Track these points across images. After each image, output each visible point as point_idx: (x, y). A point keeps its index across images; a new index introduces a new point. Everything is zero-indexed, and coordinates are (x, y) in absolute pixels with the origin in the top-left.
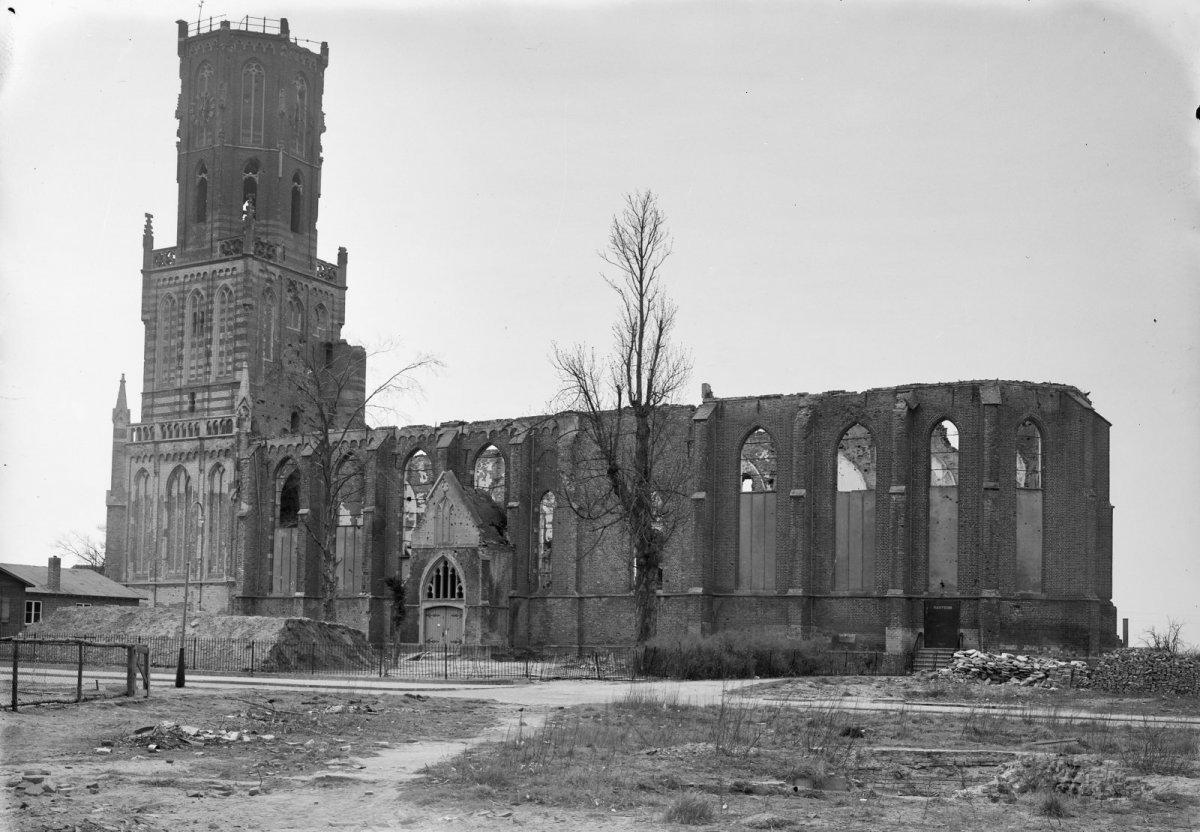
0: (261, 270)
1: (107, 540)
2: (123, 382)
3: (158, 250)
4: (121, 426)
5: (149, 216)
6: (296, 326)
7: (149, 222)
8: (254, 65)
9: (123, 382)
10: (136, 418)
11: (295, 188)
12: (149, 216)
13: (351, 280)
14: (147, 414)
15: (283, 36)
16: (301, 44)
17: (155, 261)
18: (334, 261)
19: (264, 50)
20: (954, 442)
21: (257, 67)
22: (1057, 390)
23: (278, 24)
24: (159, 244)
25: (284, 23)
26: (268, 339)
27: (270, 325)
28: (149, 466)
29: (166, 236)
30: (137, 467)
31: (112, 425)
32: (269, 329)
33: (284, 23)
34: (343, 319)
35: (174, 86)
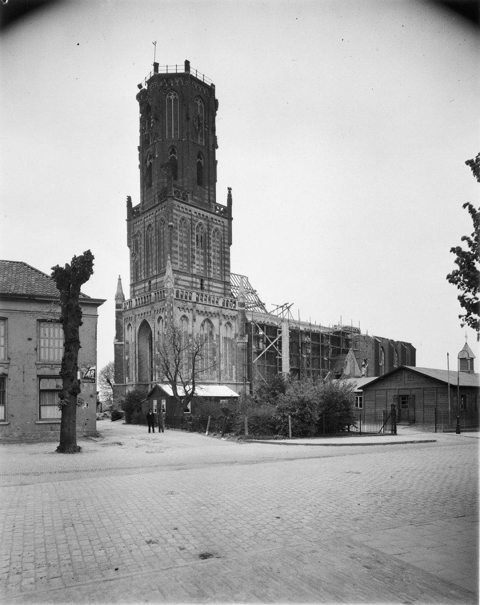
1: (115, 361)
2: (120, 279)
3: (228, 205)
4: (119, 302)
5: (230, 189)
7: (230, 192)
9: (120, 279)
10: (127, 297)
11: (199, 162)
12: (230, 189)
13: (234, 214)
14: (133, 293)
15: (187, 72)
17: (133, 213)
18: (226, 205)
19: (200, 90)
21: (175, 95)
24: (134, 205)
25: (187, 63)
28: (189, 315)
29: (136, 201)
30: (182, 313)
33: (187, 63)
34: (21, 263)
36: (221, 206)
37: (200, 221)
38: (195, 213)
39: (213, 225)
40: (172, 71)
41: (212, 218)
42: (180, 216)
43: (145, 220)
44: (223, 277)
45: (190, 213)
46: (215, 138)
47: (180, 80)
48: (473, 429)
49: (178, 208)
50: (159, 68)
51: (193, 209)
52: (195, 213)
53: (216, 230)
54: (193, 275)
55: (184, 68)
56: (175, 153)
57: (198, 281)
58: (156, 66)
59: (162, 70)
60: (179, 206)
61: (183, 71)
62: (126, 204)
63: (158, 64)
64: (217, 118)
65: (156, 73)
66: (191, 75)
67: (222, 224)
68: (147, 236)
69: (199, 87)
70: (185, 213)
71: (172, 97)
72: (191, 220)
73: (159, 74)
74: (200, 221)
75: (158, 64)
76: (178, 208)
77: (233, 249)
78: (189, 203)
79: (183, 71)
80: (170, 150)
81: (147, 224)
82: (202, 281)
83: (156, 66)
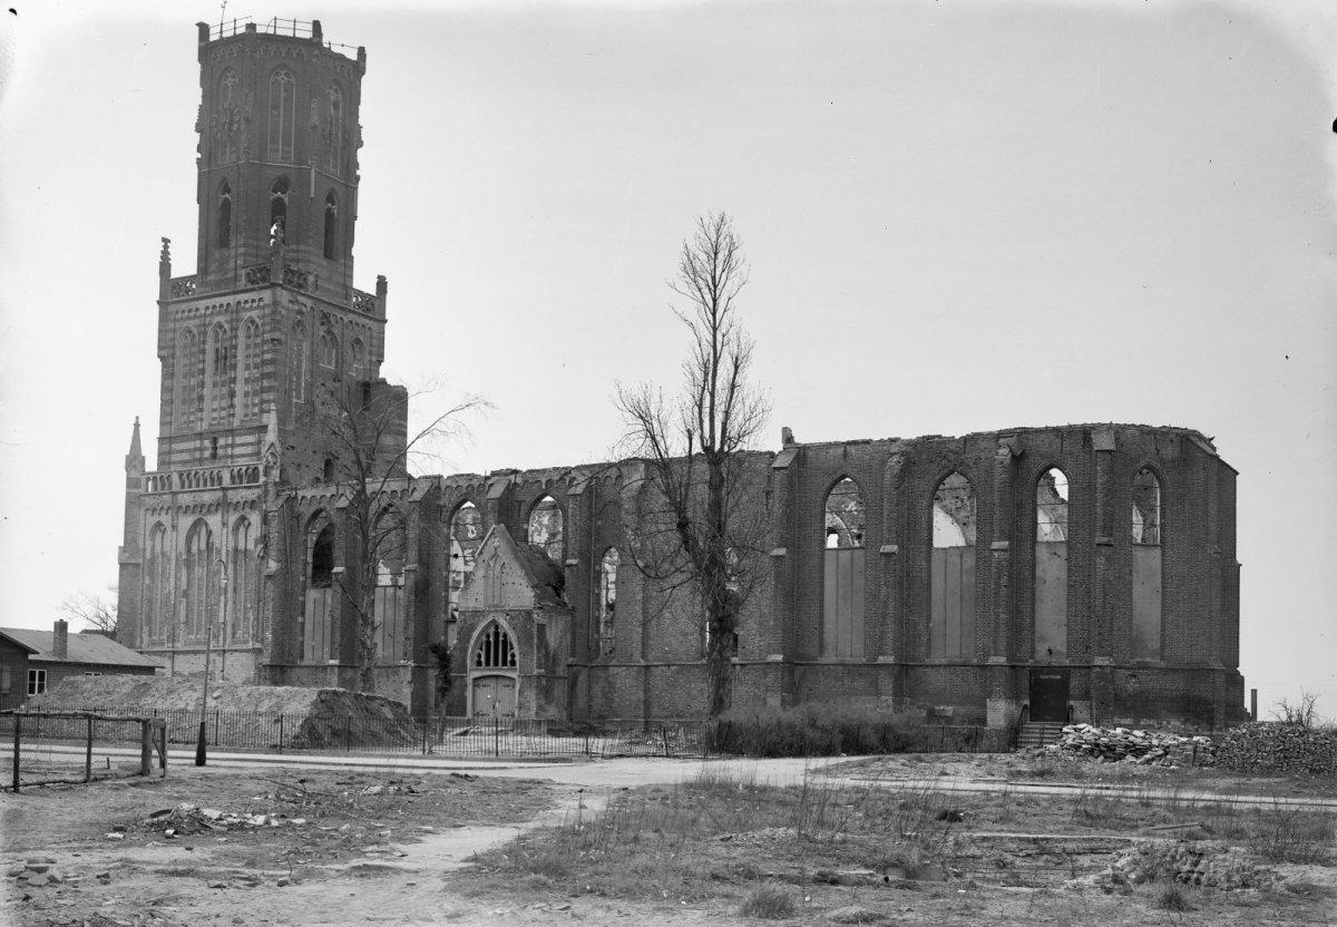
0: (291, 301)
1: (120, 602)
2: (137, 425)
3: (176, 279)
4: (135, 474)
5: (166, 241)
6: (330, 363)
7: (166, 247)
8: (283, 72)
9: (137, 425)
10: (151, 465)
11: (329, 209)
12: (166, 241)
13: (391, 312)
14: (163, 461)
15: (316, 40)
16: (335, 49)
17: (172, 291)
18: (372, 291)
21: (287, 75)
22: (1177, 435)
23: (310, 27)
24: (177, 272)
25: (317, 25)
26: (299, 378)
27: (301, 362)
28: (166, 519)
29: (185, 263)
30: (152, 520)
31: (125, 473)
32: (299, 367)
33: (317, 25)
34: (382, 355)
48: (1028, 594)
64: (194, 96)
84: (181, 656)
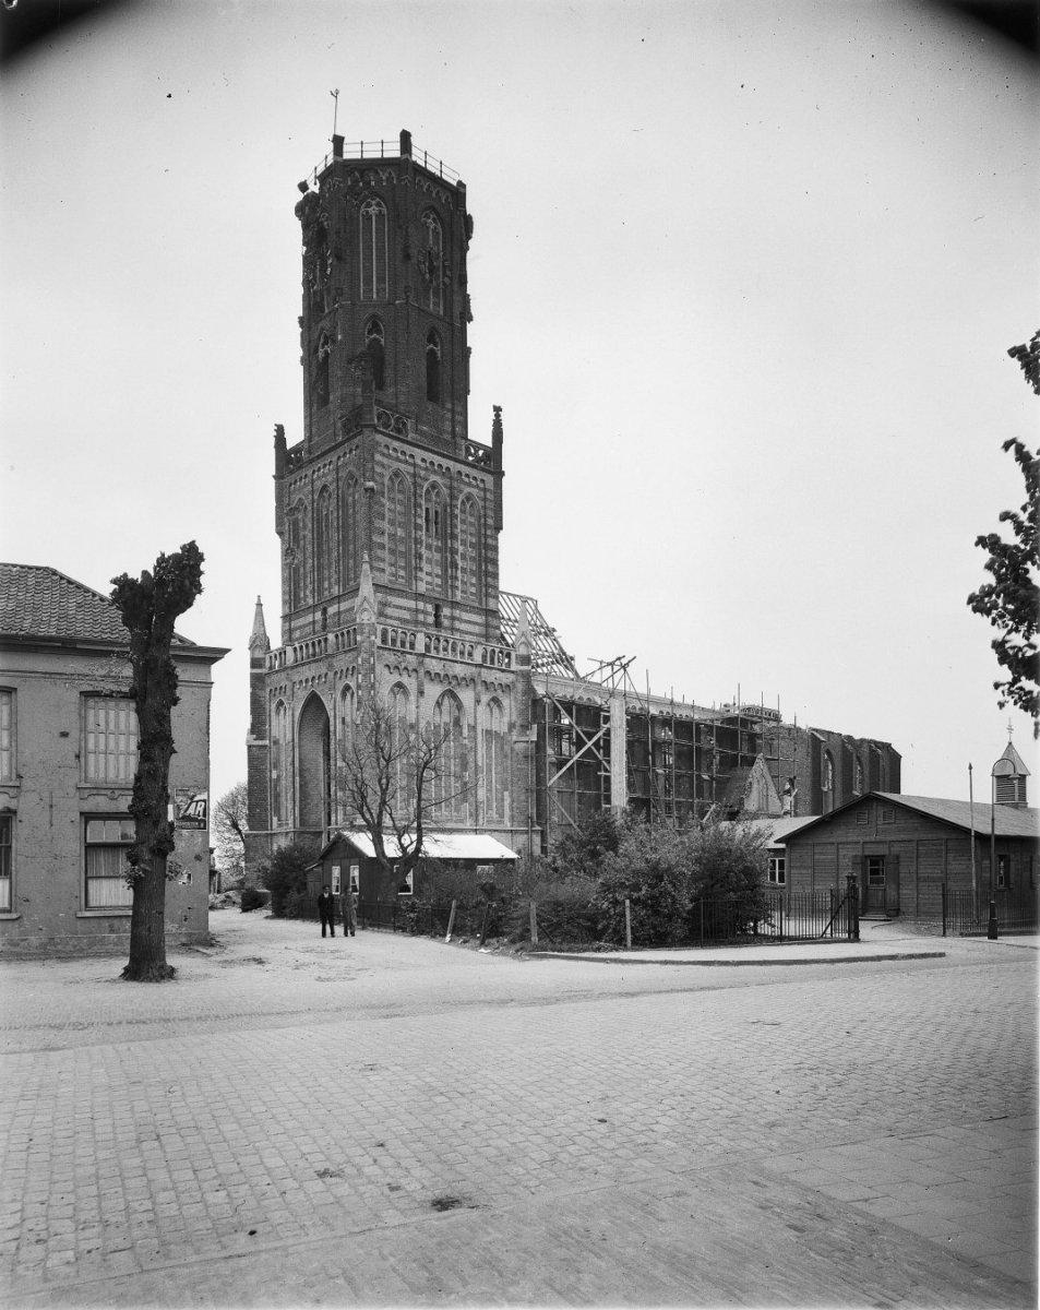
1: (250, 782)
2: (259, 605)
3: (493, 443)
4: (259, 654)
5: (497, 410)
7: (497, 416)
9: (259, 605)
10: (276, 642)
11: (432, 350)
12: (497, 410)
13: (507, 464)
14: (288, 635)
15: (405, 156)
17: (289, 462)
18: (489, 443)
20: (170, 807)
21: (378, 205)
24: (291, 443)
25: (405, 137)
28: (410, 682)
29: (295, 436)
30: (395, 678)
33: (405, 137)
34: (46, 569)
35: (470, 255)
36: (478, 446)
37: (433, 478)
38: (423, 460)
39: (462, 486)
40: (372, 153)
41: (459, 472)
42: (390, 467)
43: (315, 476)
44: (484, 599)
45: (411, 461)
46: (466, 299)
47: (390, 173)
49: (385, 451)
50: (345, 148)
51: (418, 453)
52: (423, 460)
53: (469, 497)
54: (419, 596)
55: (399, 148)
56: (379, 332)
57: (430, 608)
58: (338, 142)
59: (351, 152)
60: (387, 447)
61: (397, 154)
62: (272, 441)
63: (343, 138)
65: (339, 159)
66: (415, 163)
67: (481, 485)
68: (319, 511)
69: (432, 188)
70: (400, 461)
71: (373, 210)
72: (414, 475)
73: (345, 160)
74: (433, 478)
75: (343, 138)
76: (385, 451)
77: (505, 540)
78: (409, 439)
79: (397, 154)
80: (369, 325)
81: (319, 485)
82: (437, 608)
83: (338, 142)
84: (91, 898)
